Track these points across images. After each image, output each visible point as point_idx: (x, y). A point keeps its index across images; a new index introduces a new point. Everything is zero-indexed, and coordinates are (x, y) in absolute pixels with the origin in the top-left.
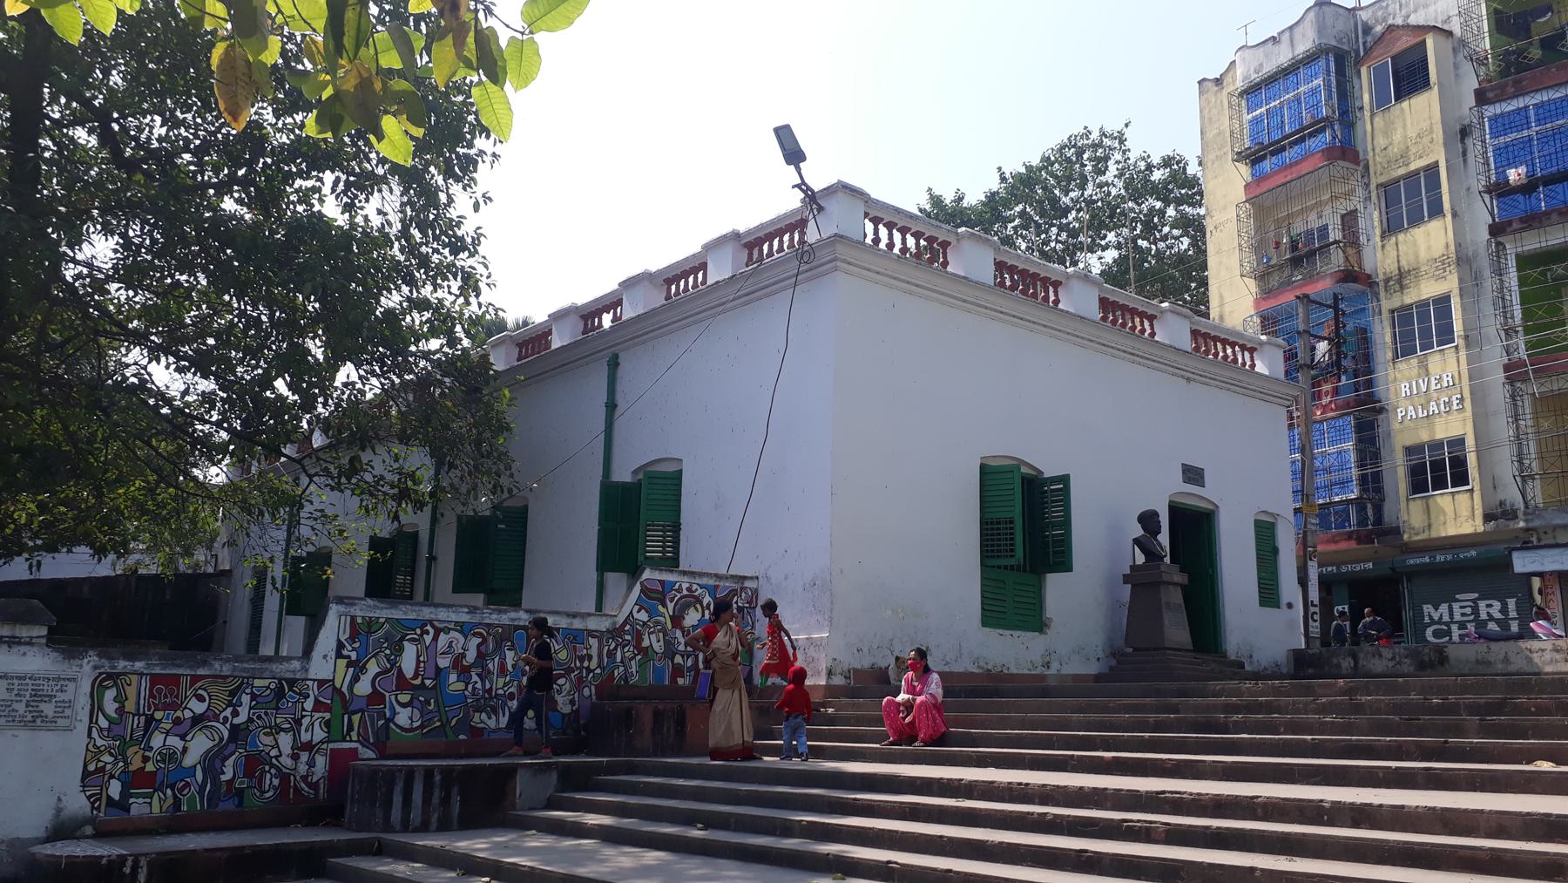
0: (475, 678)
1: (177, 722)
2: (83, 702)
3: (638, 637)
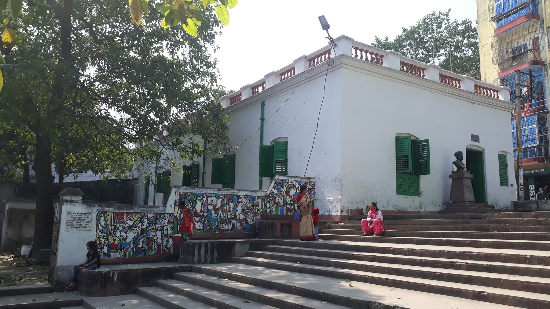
0: (220, 212)
1: (124, 228)
2: (94, 221)
3: (274, 199)
